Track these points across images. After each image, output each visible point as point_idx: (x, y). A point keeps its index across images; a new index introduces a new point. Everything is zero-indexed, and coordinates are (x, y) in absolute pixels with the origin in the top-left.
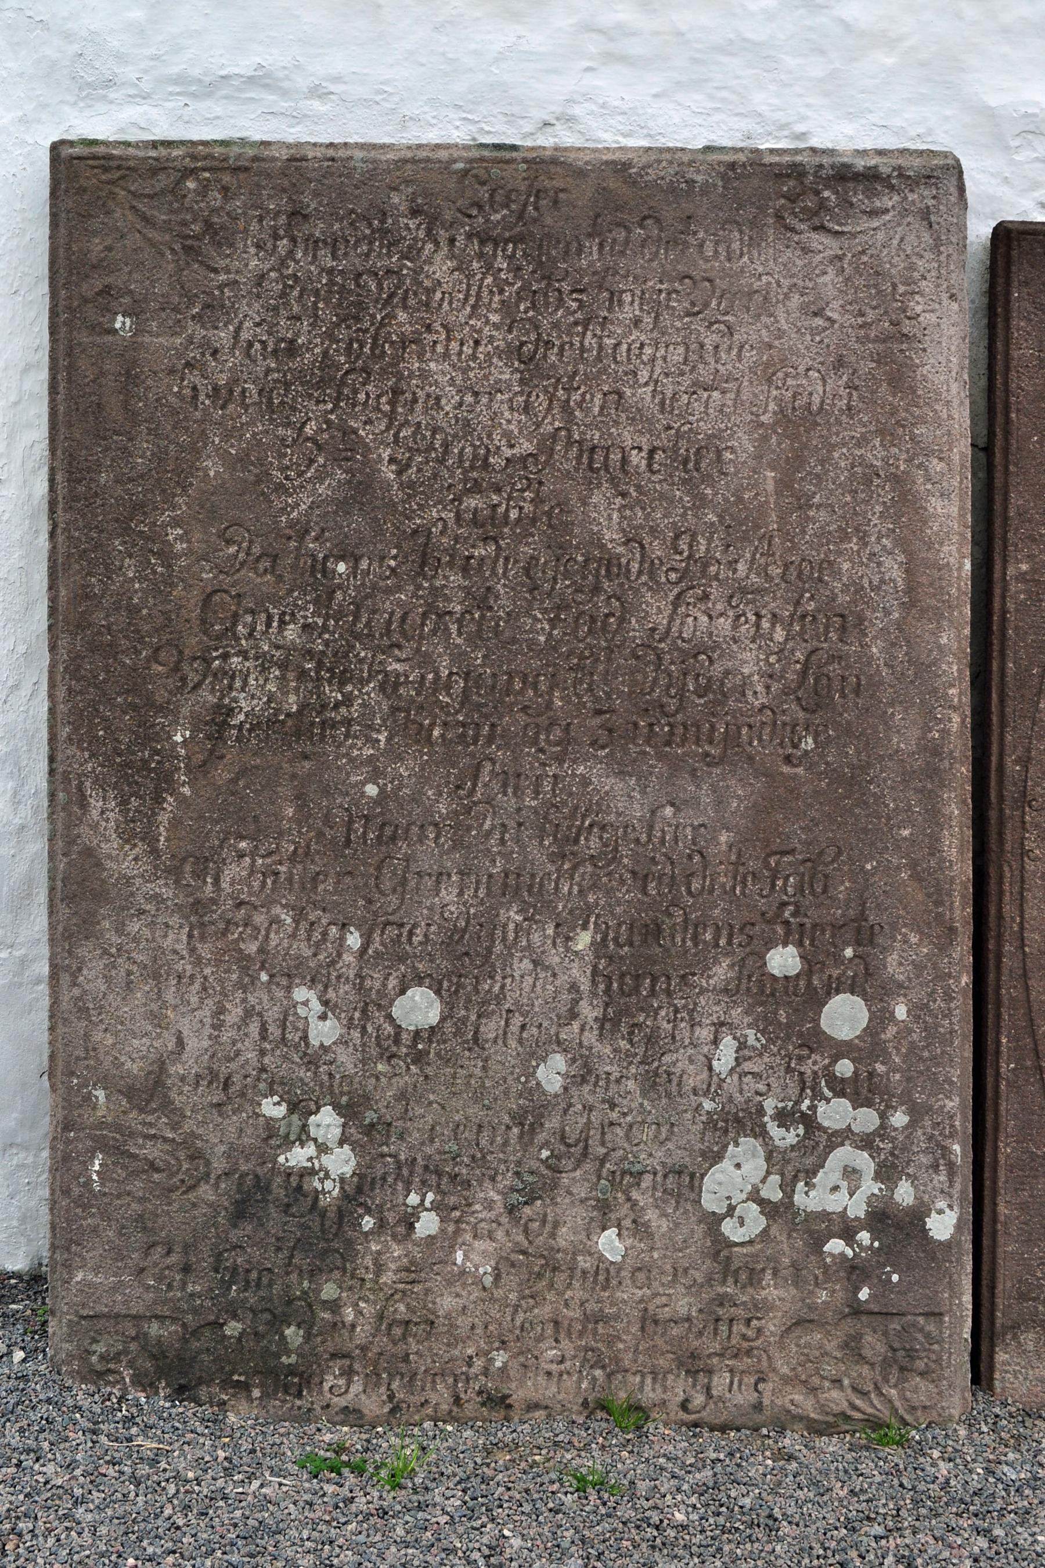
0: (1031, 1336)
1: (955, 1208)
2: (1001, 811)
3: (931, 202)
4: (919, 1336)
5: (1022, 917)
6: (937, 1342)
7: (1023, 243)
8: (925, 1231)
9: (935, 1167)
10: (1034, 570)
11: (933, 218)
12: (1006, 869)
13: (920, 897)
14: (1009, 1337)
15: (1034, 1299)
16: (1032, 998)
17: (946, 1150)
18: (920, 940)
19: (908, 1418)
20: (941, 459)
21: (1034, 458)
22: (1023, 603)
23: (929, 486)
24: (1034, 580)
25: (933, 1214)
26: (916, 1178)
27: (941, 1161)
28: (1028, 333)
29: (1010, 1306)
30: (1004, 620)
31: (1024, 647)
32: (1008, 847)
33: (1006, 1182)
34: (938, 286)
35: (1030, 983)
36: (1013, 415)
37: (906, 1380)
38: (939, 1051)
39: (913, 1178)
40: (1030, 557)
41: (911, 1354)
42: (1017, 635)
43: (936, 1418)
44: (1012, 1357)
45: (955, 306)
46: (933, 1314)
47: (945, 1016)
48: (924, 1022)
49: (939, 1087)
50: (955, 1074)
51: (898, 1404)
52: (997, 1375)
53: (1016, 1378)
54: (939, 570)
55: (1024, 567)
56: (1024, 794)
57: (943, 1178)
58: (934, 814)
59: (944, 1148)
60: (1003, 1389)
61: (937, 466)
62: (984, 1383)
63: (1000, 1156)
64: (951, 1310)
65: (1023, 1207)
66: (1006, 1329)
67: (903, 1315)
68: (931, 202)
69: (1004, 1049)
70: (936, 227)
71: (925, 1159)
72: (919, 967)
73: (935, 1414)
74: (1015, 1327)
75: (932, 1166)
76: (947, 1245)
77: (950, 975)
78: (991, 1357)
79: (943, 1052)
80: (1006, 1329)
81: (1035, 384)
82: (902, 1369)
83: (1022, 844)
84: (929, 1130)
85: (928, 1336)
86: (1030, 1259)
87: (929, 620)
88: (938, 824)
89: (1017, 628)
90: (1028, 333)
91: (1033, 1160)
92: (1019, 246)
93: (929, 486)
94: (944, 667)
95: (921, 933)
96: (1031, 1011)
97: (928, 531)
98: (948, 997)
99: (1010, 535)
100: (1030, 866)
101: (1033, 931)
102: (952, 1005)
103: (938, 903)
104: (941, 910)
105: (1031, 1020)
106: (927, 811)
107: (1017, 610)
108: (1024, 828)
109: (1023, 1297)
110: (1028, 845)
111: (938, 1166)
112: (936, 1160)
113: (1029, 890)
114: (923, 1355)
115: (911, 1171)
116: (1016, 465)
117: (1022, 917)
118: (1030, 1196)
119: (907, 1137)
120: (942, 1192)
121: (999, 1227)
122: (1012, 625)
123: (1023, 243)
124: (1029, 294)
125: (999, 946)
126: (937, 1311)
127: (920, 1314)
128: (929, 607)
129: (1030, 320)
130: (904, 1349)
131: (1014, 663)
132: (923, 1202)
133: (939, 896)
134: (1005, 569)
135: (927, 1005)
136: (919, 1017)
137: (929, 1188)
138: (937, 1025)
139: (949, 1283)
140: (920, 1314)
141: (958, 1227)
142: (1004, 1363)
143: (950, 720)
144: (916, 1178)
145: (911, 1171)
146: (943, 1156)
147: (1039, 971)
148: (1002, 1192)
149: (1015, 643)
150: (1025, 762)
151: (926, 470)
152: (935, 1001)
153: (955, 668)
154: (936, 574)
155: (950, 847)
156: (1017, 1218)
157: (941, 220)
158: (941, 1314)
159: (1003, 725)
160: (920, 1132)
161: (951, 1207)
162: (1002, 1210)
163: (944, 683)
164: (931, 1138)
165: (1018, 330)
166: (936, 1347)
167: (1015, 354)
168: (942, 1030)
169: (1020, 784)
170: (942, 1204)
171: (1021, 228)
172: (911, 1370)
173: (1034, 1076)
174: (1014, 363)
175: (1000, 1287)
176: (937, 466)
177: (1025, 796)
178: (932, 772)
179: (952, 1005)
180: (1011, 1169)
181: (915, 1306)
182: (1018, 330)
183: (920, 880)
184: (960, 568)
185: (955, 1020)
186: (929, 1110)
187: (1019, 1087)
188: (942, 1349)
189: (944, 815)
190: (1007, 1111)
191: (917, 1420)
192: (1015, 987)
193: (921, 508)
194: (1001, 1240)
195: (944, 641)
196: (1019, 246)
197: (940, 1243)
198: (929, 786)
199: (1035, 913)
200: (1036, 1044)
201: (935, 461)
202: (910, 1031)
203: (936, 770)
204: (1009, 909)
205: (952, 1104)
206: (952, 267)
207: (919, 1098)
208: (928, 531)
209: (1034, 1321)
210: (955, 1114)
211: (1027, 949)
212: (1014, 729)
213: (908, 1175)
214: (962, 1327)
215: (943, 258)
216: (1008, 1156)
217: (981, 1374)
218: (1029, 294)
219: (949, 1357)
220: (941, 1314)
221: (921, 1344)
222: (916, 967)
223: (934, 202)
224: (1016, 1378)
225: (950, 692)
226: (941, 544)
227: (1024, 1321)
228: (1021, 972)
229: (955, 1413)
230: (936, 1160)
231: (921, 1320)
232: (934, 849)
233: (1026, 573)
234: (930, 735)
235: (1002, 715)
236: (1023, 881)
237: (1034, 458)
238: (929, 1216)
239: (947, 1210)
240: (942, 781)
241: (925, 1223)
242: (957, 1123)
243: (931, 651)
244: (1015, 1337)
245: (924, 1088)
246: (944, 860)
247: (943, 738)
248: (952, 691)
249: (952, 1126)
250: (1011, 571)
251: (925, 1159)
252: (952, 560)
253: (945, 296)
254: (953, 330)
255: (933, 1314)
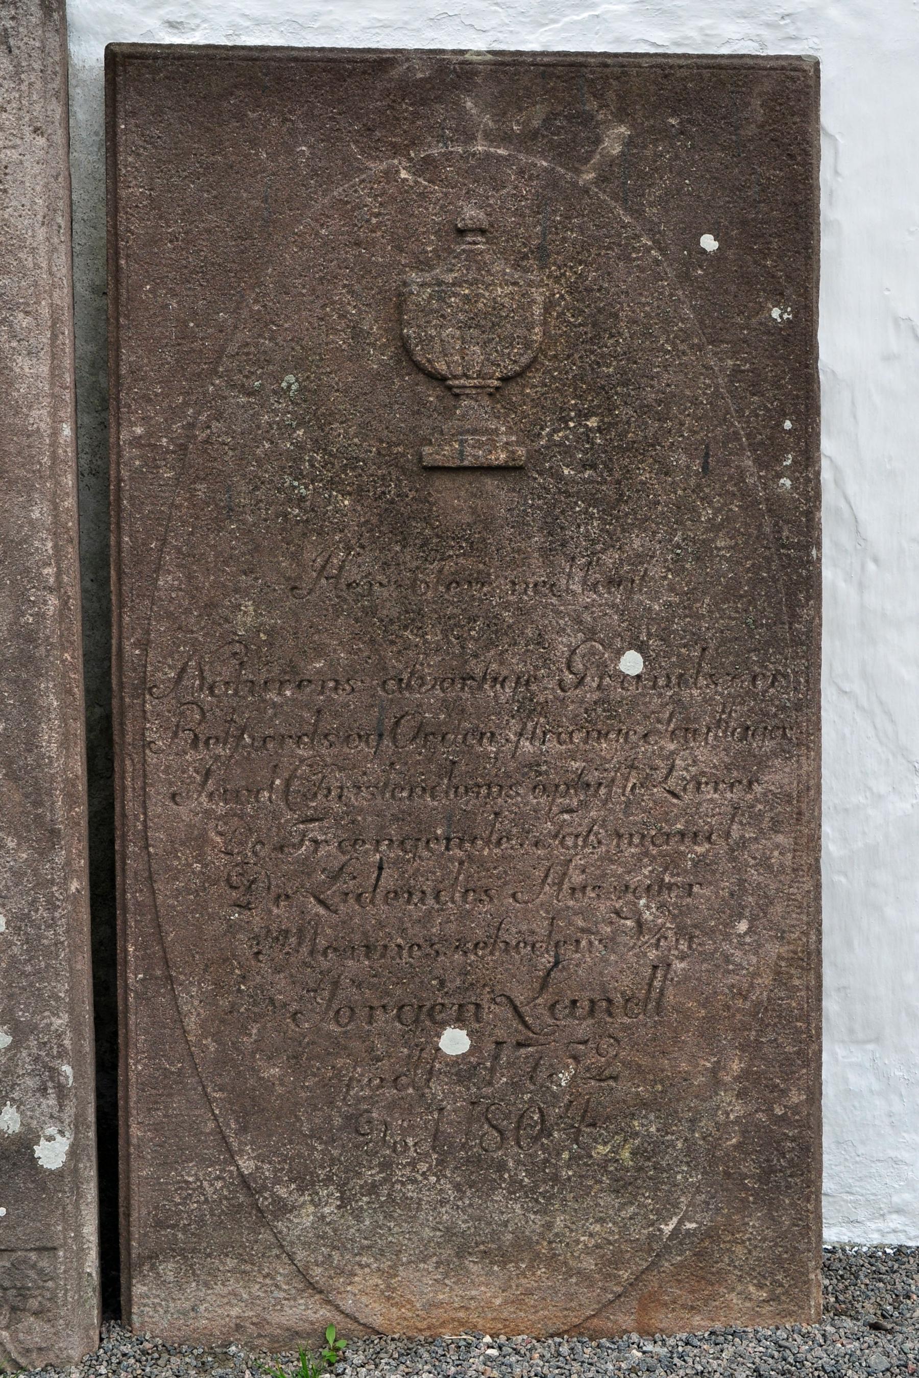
0: (171, 1266)
1: (67, 1134)
2: (122, 699)
3: (9, 24)
4: (32, 1273)
5: (145, 814)
6: (52, 1279)
7: (130, 69)
8: (33, 1160)
9: (43, 1090)
10: (149, 434)
11: (12, 42)
12: (128, 762)
13: (17, 797)
14: (146, 1268)
15: (173, 1227)
16: (159, 902)
17: (54, 1072)
18: (19, 844)
19: (22, 1361)
20: (27, 313)
21: (147, 309)
22: (138, 471)
23: (14, 344)
24: (150, 445)
25: (43, 1141)
26: (22, 1103)
27: (50, 1084)
28: (137, 170)
29: (146, 1235)
30: (119, 489)
31: (141, 519)
32: (129, 738)
33: (138, 1102)
34: (19, 119)
35: (156, 886)
36: (123, 262)
37: (19, 1321)
38: (43, 964)
39: (19, 1104)
40: (145, 419)
41: (23, 1293)
42: (132, 505)
43: (54, 1361)
44: (150, 1289)
45: (41, 141)
46: (45, 1249)
47: (49, 926)
48: (26, 933)
49: (44, 1003)
50: (62, 989)
51: (10, 1347)
52: (135, 1309)
53: (156, 1311)
54: (29, 436)
55: (139, 430)
56: (144, 680)
57: (52, 1101)
58: (31, 707)
59: (52, 1070)
60: (142, 1324)
61: (22, 321)
62: (124, 1317)
63: (131, 1074)
64: (65, 1243)
65: (157, 1128)
66: (142, 1260)
67: (12, 1251)
68: (9, 24)
69: (131, 958)
70: (16, 51)
71: (31, 1083)
72: (18, 875)
73: (52, 1355)
74: (152, 1257)
75: (39, 1090)
76: (59, 1174)
77: (52, 882)
78: (129, 1289)
79: (48, 966)
80: (142, 1260)
81: (146, 226)
82: (14, 1309)
83: (143, 734)
84: (35, 1051)
85: (41, 1272)
86: (167, 1183)
87: (19, 492)
88: (34, 717)
89: (132, 498)
90: (137, 170)
91: (166, 1077)
92: (125, 71)
93: (14, 344)
94: (37, 544)
95: (20, 837)
96: (158, 917)
97: (15, 394)
98: (52, 906)
99: (122, 395)
100: (152, 759)
101: (157, 830)
102: (57, 915)
103: (37, 804)
104: (40, 811)
105: (159, 926)
106: (22, 703)
107: (131, 478)
108: (145, 718)
109: (160, 1224)
110: (150, 736)
111: (45, 1089)
112: (44, 1083)
113: (152, 785)
114: (36, 1293)
115: (16, 1095)
116: (127, 317)
117: (145, 814)
118: (165, 1116)
119: (10, 1059)
120: (52, 1117)
121: (132, 1150)
122: (127, 495)
123: (130, 69)
124: (137, 126)
125: (124, 847)
126: (50, 1245)
127: (31, 1250)
128: (18, 478)
129: (139, 155)
130: (15, 1287)
131: (130, 536)
132: (30, 1129)
133: (38, 795)
134: (119, 432)
135: (28, 916)
136: (20, 928)
137: (37, 1114)
138: (40, 937)
139: (63, 1214)
140: (31, 1250)
141: (74, 1153)
142: (142, 1296)
143: (45, 603)
144: (22, 1103)
145: (16, 1095)
146: (51, 1078)
147: (166, 872)
148: (134, 1112)
149: (130, 515)
150: (144, 645)
151: (11, 326)
152: (37, 910)
153: (50, 545)
154: (25, 441)
155: (49, 742)
156: (151, 1140)
157: (21, 44)
158: (55, 1249)
159: (121, 605)
160: (24, 1053)
161: (61, 1132)
162: (135, 1131)
163: (37, 563)
164: (37, 1059)
165: (126, 166)
166: (50, 1284)
167: (123, 193)
168: (45, 942)
169: (140, 669)
170: (51, 1130)
171: (126, 50)
172: (24, 1310)
173: (165, 986)
174: (122, 203)
175: (135, 1215)
176: (22, 321)
177: (145, 683)
178: (27, 660)
179: (57, 915)
180: (142, 1088)
181: (25, 1242)
182: (126, 166)
183: (16, 779)
184: (55, 433)
185: (60, 931)
186: (33, 1028)
187: (149, 999)
188: (58, 1285)
189: (41, 708)
190: (137, 1025)
191: (32, 1363)
192: (141, 891)
193: (6, 367)
194: (134, 1164)
195: (36, 515)
196: (125, 71)
197: (51, 1172)
198: (24, 676)
199: (160, 810)
200: (165, 952)
201: (21, 316)
202: (10, 944)
203: (31, 658)
204: (132, 807)
205: (60, 1022)
206: (35, 97)
207: (22, 1016)
208: (15, 394)
209: (174, 1250)
210: (64, 1033)
211: (151, 850)
212: (132, 609)
213: (13, 1100)
214: (81, 1260)
215: (24, 87)
216: (139, 1074)
217: (113, 1303)
218: (137, 126)
219: (65, 1294)
220: (55, 1249)
221: (35, 1281)
222: (14, 874)
223: (13, 23)
224: (156, 1311)
225: (45, 571)
226: (30, 407)
227: (162, 1250)
228: (146, 875)
229: (75, 1354)
230: (44, 1083)
231: (33, 1256)
232: (31, 745)
233: (140, 437)
234: (22, 620)
235: (120, 594)
236: (145, 776)
237: (147, 309)
238: (37, 1144)
239: (58, 1137)
240: (38, 669)
241: (33, 1151)
242: (67, 1042)
243: (21, 526)
244: (153, 1268)
245: (27, 1005)
246: (43, 756)
247: (38, 622)
248: (47, 571)
249: (61, 1046)
250: (124, 435)
251: (31, 1083)
252: (43, 426)
253: (27, 130)
254: (37, 169)
255: (45, 1249)
